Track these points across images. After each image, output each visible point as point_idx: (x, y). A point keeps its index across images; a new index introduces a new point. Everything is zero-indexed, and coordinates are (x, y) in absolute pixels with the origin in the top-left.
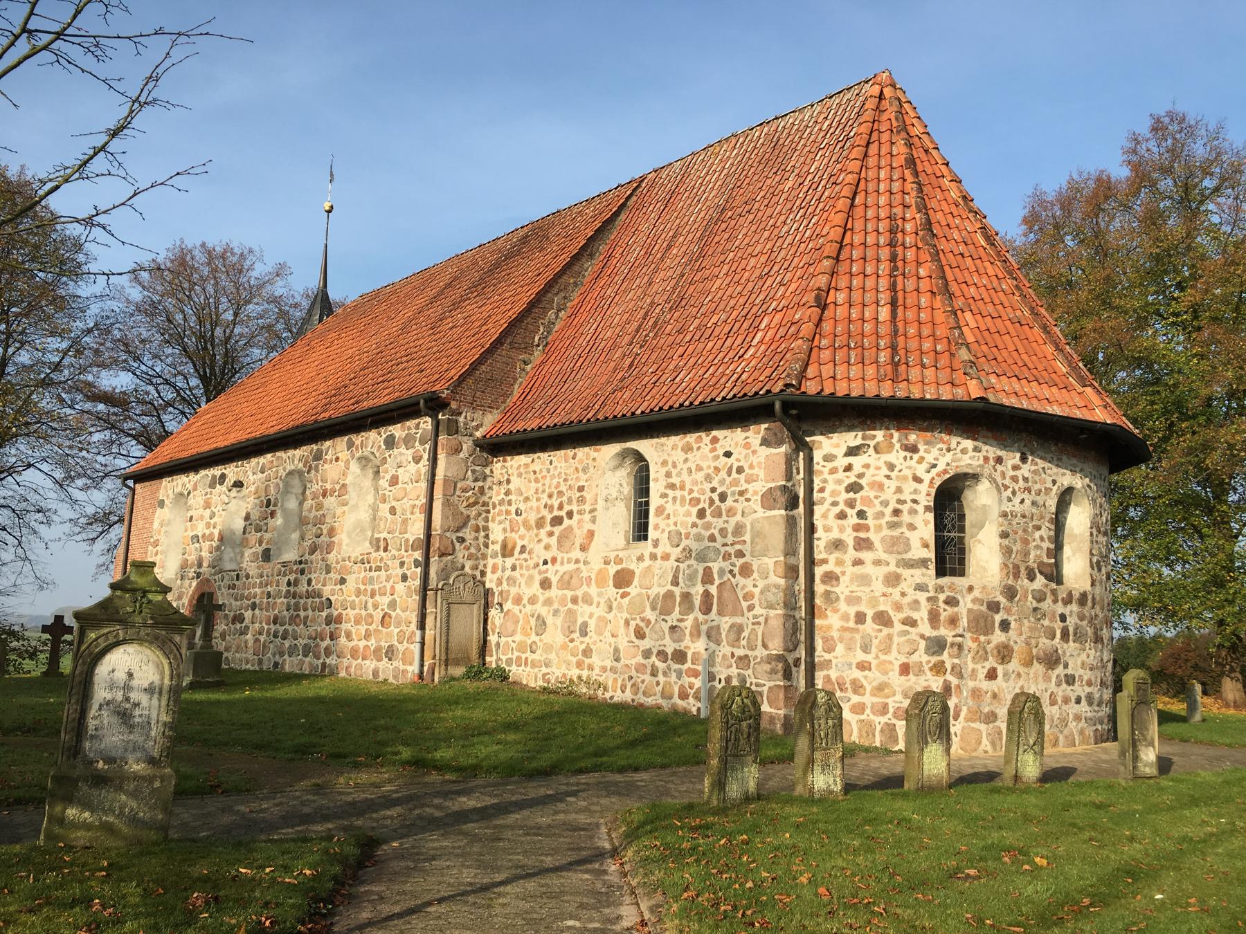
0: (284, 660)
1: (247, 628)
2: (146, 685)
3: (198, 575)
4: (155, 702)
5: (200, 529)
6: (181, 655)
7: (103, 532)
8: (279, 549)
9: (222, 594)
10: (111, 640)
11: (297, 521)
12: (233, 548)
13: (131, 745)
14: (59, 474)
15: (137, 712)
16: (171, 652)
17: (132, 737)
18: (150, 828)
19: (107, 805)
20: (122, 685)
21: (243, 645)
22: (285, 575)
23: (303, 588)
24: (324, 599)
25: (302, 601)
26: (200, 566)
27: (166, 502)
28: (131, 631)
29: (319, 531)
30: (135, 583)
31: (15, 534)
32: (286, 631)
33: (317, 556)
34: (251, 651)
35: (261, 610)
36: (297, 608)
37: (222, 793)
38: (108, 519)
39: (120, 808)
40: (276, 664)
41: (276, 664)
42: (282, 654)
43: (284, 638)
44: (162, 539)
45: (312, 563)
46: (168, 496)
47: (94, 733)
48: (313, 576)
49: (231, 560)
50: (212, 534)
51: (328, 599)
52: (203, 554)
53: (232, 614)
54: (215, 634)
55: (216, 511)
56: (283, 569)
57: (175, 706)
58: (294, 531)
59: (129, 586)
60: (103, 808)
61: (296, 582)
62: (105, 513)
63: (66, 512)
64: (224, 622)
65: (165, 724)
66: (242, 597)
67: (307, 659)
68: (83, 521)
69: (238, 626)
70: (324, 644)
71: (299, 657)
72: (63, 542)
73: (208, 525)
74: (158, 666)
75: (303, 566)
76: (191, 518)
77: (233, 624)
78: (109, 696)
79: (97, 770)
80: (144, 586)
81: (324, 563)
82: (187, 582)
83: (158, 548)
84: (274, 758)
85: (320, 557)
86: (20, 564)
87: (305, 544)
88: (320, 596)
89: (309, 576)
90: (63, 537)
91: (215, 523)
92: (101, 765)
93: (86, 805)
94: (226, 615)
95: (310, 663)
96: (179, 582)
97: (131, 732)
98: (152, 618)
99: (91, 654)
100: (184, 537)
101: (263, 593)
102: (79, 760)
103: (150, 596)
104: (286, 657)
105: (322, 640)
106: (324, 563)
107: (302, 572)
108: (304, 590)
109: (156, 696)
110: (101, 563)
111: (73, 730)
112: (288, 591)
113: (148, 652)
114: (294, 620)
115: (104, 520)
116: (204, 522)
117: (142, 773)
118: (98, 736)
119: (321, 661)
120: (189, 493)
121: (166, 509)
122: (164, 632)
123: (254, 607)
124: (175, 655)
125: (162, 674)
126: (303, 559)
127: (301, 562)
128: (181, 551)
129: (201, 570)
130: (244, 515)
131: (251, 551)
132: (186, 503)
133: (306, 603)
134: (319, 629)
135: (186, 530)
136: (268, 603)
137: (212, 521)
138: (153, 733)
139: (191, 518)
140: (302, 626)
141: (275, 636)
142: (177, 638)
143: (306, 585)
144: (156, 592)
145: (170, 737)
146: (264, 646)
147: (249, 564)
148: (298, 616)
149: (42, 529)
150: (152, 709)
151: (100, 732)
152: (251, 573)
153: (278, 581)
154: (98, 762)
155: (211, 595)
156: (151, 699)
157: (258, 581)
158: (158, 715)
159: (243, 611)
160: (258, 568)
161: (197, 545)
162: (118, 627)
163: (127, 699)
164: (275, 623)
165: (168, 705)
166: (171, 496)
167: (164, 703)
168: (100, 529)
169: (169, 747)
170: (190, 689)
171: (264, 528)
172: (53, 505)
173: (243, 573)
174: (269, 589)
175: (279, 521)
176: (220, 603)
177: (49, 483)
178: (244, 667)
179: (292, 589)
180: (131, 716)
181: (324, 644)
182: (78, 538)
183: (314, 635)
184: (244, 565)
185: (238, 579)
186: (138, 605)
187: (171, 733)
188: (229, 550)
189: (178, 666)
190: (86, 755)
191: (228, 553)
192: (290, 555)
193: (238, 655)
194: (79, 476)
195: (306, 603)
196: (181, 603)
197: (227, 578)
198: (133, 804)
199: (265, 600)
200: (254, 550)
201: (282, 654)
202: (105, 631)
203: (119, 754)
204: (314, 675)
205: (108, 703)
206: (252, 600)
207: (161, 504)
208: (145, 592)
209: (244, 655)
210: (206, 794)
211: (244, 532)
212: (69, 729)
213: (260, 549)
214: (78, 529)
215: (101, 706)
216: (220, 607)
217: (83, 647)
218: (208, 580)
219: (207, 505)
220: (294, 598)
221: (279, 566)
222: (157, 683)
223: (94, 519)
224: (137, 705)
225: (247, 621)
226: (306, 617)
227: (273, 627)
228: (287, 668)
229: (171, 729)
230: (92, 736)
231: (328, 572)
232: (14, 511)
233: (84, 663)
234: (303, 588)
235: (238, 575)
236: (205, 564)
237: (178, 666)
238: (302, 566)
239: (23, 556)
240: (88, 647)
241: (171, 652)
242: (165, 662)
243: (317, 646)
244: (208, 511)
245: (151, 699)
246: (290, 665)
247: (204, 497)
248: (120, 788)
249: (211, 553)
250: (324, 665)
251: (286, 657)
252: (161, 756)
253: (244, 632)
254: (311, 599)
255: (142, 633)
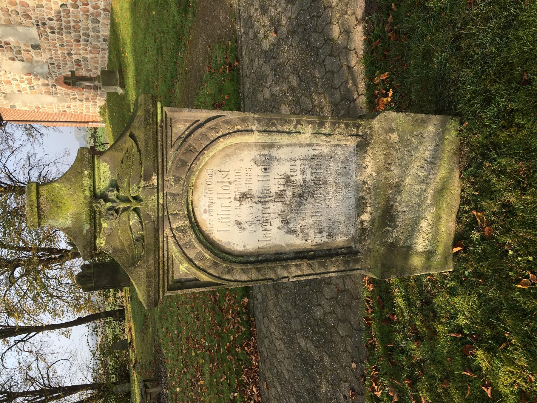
0: (102, 35)
1: (83, 58)
2: (258, 170)
3: (54, 85)
4: (282, 153)
5: (25, 86)
6: (209, 120)
7: (36, 130)
8: (31, 39)
9: (64, 72)
10: (191, 237)
11: (8, 28)
12: (34, 67)
13: (341, 179)
14: (8, 153)
15: (298, 178)
16: (204, 136)
17: (331, 181)
18: (442, 139)
19: (416, 200)
20: (260, 206)
21: (94, 60)
22: (47, 35)
23: (55, 23)
24: (61, 9)
25: (64, 24)
26: (48, 85)
27: (11, 104)
28: (173, 208)
29: (14, 12)
30: (77, 217)
31: (43, 168)
32: (84, 34)
33: (31, 13)
34: (97, 55)
35: (71, 50)
36: (68, 28)
37: (238, 61)
38: (29, 129)
39: (420, 183)
40: (105, 40)
41: (105, 40)
42: (98, 37)
43: (88, 35)
44: (34, 105)
45: (37, 18)
46: (7, 104)
47: (325, 234)
48: (46, 17)
49: (42, 68)
50: (27, 79)
51: (61, 6)
52: (40, 84)
53: (75, 67)
54: (88, 75)
55: (11, 78)
56: (44, 36)
57: (290, 122)
58: (16, 30)
59: (87, 227)
60: (419, 205)
61: (51, 28)
62: (26, 130)
63: (28, 148)
64: (80, 70)
65: (316, 134)
66: (64, 61)
67: (101, 20)
68: (31, 139)
69: (82, 63)
70: (91, 10)
71: (100, 26)
72: (44, 147)
73: (22, 82)
74: (228, 156)
75: (40, 23)
76: (18, 91)
77: (81, 65)
78: (277, 222)
79: (372, 221)
80: (82, 201)
81: (36, 9)
82: (58, 91)
83: (40, 106)
84: (190, 28)
85: (32, 12)
86: (57, 164)
87: (24, 22)
88: (59, 12)
89: (46, 19)
90: (41, 147)
91: (19, 77)
92: (366, 217)
93: (414, 226)
94: (76, 70)
95: (103, 19)
96: (59, 95)
97: (325, 183)
98: (147, 178)
99: (215, 264)
100: (31, 93)
101: (61, 49)
102: (359, 246)
103: (102, 185)
104: (100, 34)
105: (88, 11)
106: (36, 9)
107: (44, 24)
108: (56, 22)
109: (274, 153)
110: (53, 130)
111: (322, 265)
112: (58, 33)
113: (205, 175)
114: (76, 29)
115: (30, 131)
116: (20, 84)
117: (380, 159)
118: (330, 227)
119: (102, 12)
120: (3, 93)
121: (16, 104)
122: (171, 152)
123: (70, 54)
124: (211, 129)
125: (240, 147)
126: (35, 23)
127: (38, 25)
128: (40, 95)
129: (50, 84)
130: (11, 61)
131: (34, 56)
132: (10, 94)
133: (65, 22)
134: (81, 13)
135: (27, 93)
136: (67, 45)
137: (19, 79)
138: (326, 150)
139: (18, 91)
140: (80, 24)
141: (87, 41)
142: (180, 128)
143: (53, 22)
144: (92, 176)
145: (334, 124)
146: (94, 47)
147: (43, 57)
148: (73, 27)
149: (38, 157)
150: (293, 156)
151: (325, 225)
152: (49, 56)
153: (52, 40)
154: (362, 222)
155: (66, 78)
156: (279, 160)
157: (53, 52)
158: (301, 146)
159: (73, 60)
160: (45, 52)
161: (35, 87)
162: (167, 231)
163: (280, 195)
164: (79, 41)
165: (289, 133)
166: (7, 102)
167: (284, 139)
168: (35, 132)
169: (347, 125)
170: (124, 87)
171: (18, 49)
172: (24, 156)
173: (50, 61)
174: (58, 45)
175: (11, 40)
176: (70, 73)
177: (12, 158)
178: (106, 59)
179: (56, 31)
180: (304, 185)
181: (91, 10)
182: (41, 141)
183: (86, 16)
184: (44, 60)
185: (54, 64)
186: (122, 206)
187: (328, 124)
188: (36, 69)
189: (227, 122)
190: (353, 238)
191: (38, 70)
192: (34, 32)
193: (100, 62)
194: (8, 143)
195: (65, 22)
196: (71, 94)
197: (53, 70)
198: (413, 171)
199: (65, 47)
200: (33, 55)
201: (98, 37)
202: (174, 250)
203: (352, 194)
204: (112, 16)
205: (286, 222)
206: (66, 55)
207: (13, 107)
208: (95, 196)
209: (100, 59)
210: (239, 74)
211: (23, 61)
212: (323, 270)
213: (33, 52)
214: (36, 141)
215: (291, 232)
216: (73, 73)
217: (204, 278)
218: (56, 80)
219: (9, 82)
220: (62, 29)
221: (42, 39)
222: (255, 153)
223: (30, 135)
224: (287, 180)
225: (79, 58)
226: (74, 21)
227: (82, 42)
228: (107, 33)
229: (322, 124)
230: (330, 235)
231: (42, 6)
232: (30, 170)
233: (229, 271)
234: (55, 23)
235: (51, 64)
236: (47, 82)
237: (227, 122)
238: (40, 24)
239: (53, 163)
240: (204, 271)
241: (204, 136)
242: (222, 143)
243: (92, 14)
244: (12, 82)
245: (279, 160)
246: (105, 32)
247: (4, 85)
248: (398, 188)
249: (39, 79)
250: (105, 10)
251: (100, 34)
252: (357, 135)
253: (86, 60)
254: (62, 18)
255: (176, 189)
